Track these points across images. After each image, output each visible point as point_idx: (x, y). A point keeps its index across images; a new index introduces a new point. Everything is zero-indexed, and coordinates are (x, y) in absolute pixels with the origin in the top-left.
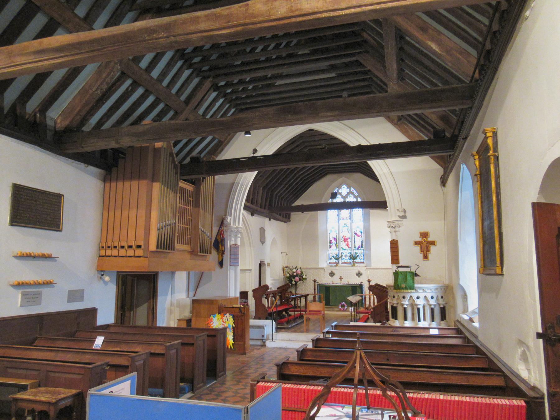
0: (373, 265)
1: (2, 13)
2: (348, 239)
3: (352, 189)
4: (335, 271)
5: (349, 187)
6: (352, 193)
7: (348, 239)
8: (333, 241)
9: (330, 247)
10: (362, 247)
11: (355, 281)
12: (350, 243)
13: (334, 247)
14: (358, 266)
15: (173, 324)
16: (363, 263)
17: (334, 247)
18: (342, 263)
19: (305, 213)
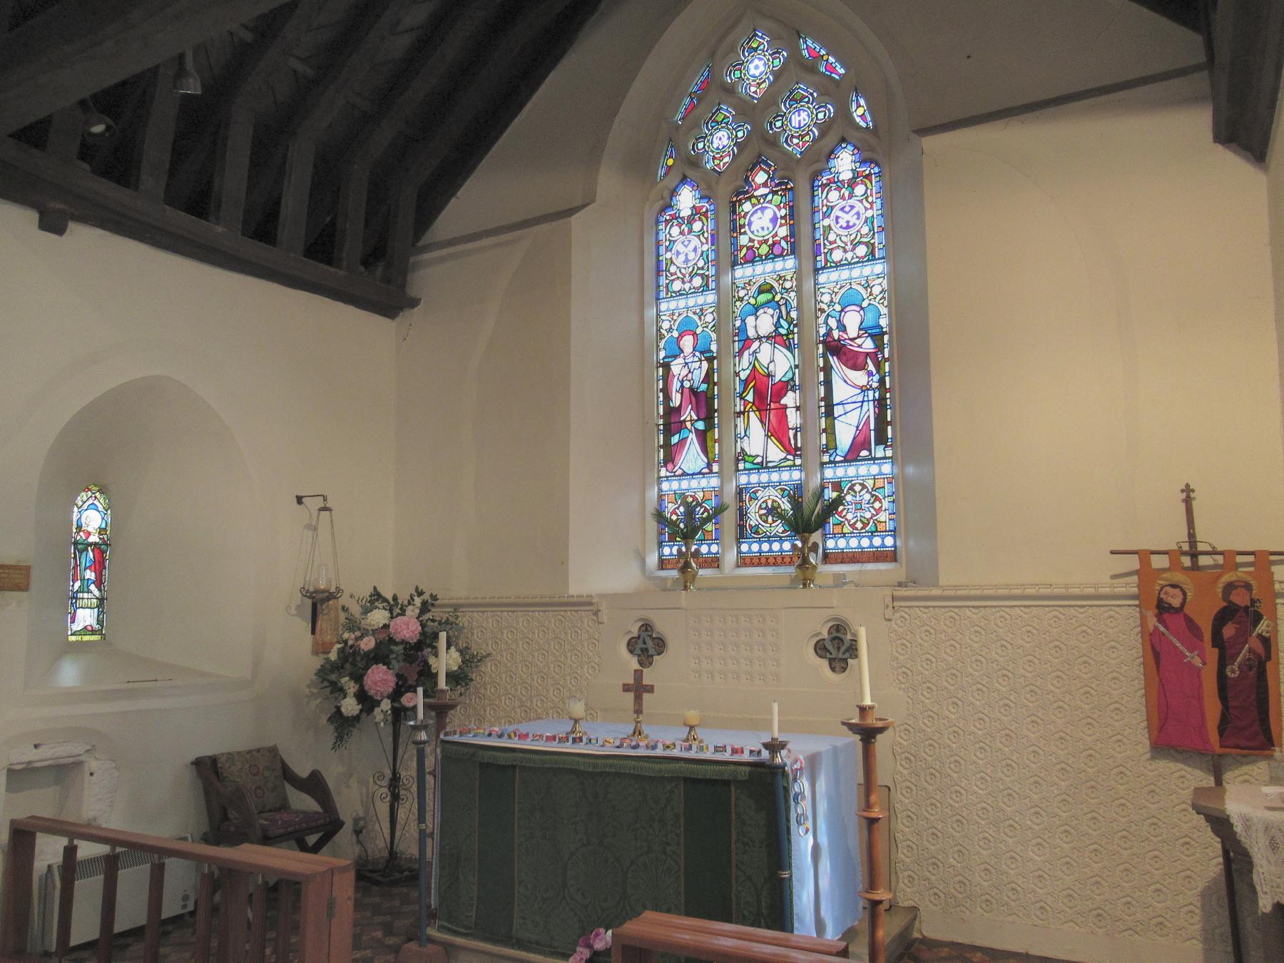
0: (950, 575)
1: (1134, 5)
2: (783, 388)
3: (808, 46)
4: (663, 626)
5: (787, 33)
6: (809, 67)
7: (783, 388)
8: (688, 414)
9: (670, 459)
10: (881, 440)
11: (706, 714)
12: (793, 419)
13: (692, 457)
14: (840, 581)
15: (1212, 778)
16: (891, 556)
17: (692, 457)
18: (744, 561)
19: (82, 236)
